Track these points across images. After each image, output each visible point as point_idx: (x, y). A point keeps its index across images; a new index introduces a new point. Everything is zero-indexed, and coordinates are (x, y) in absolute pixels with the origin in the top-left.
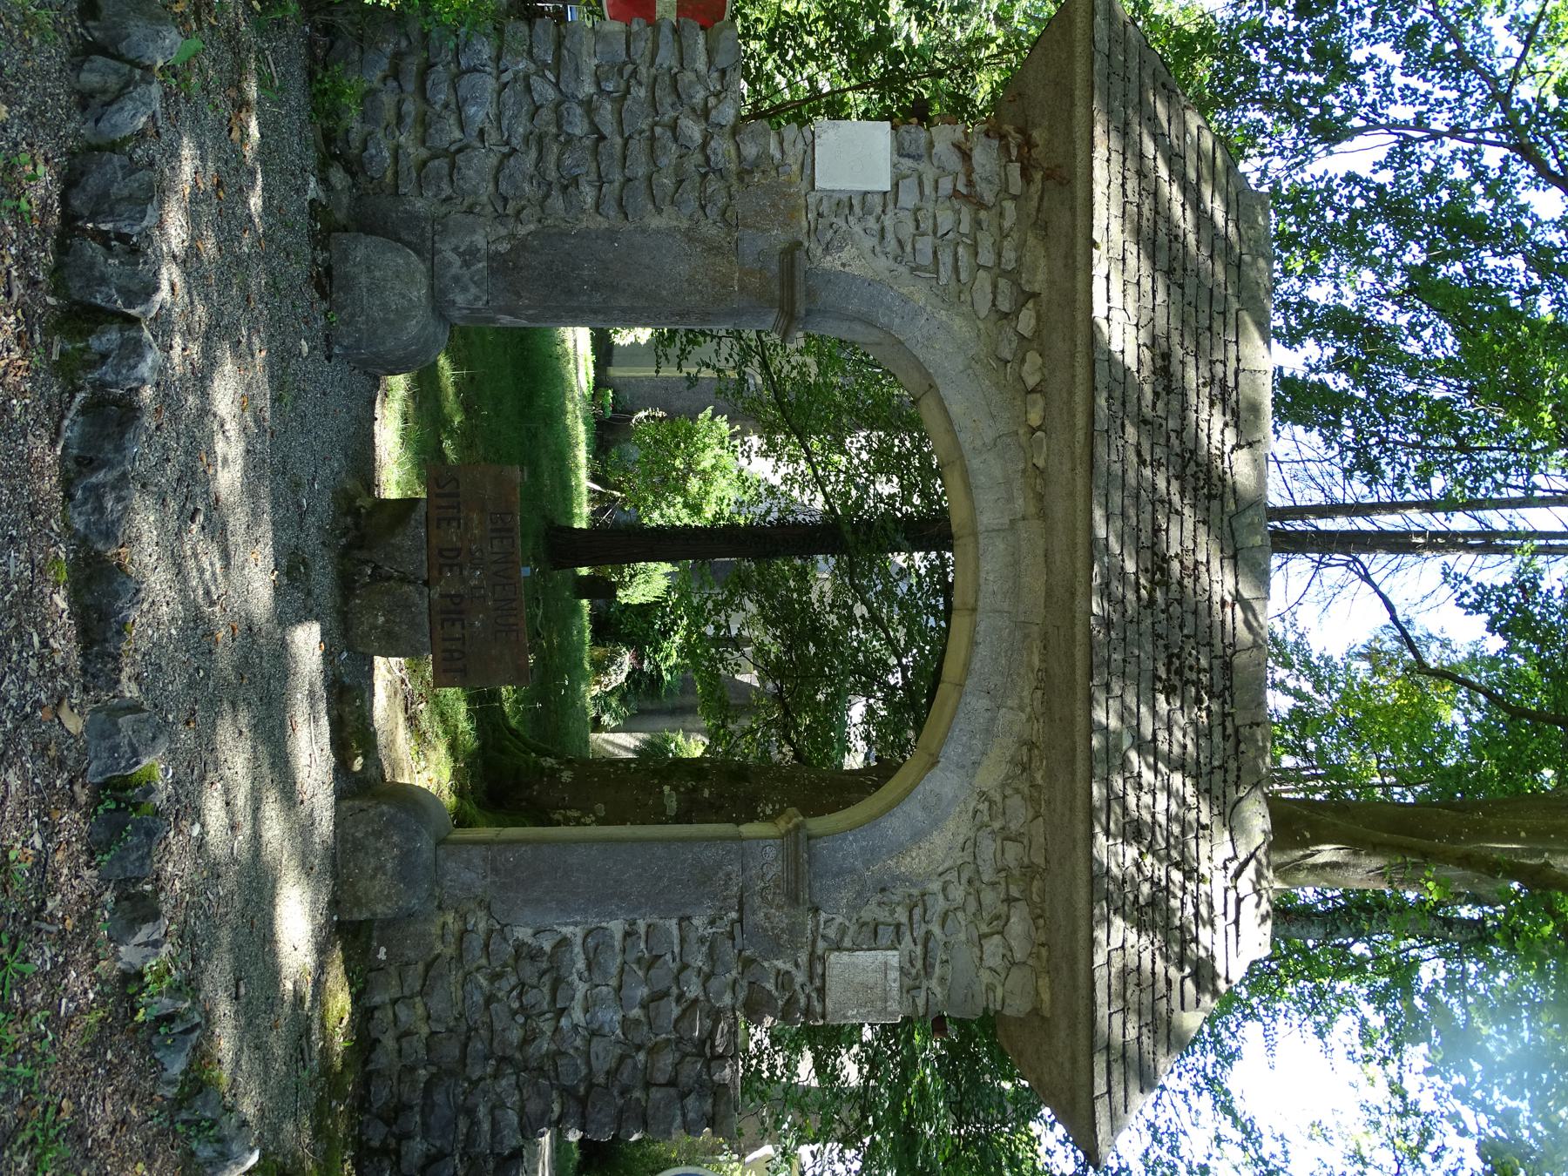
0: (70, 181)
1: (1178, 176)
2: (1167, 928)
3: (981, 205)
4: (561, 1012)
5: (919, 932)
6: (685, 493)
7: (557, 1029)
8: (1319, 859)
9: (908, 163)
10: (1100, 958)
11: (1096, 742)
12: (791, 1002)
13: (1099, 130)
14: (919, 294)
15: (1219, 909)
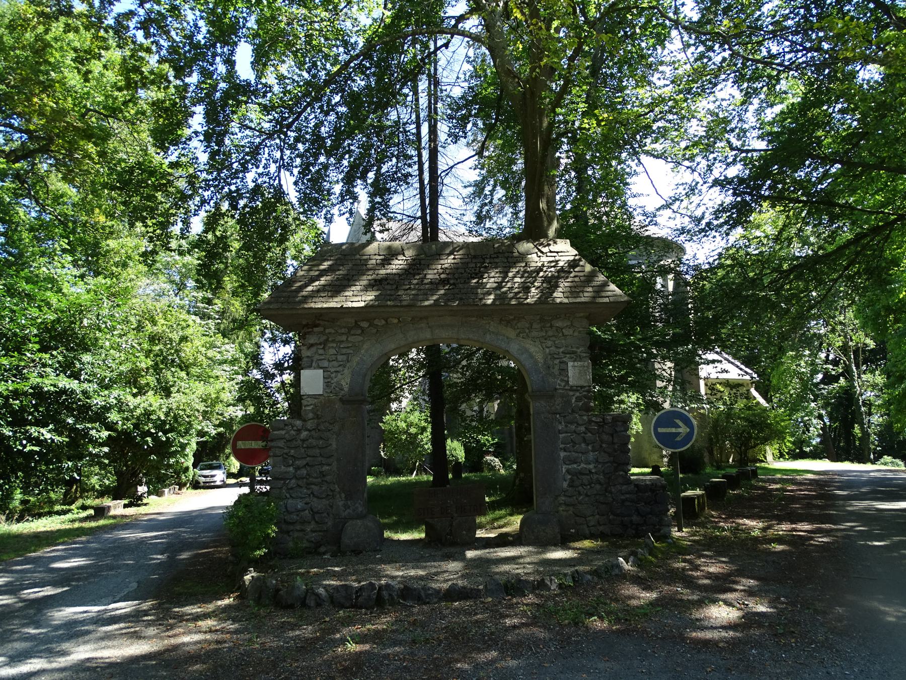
0: (342, 607)
1: (317, 278)
2: (559, 277)
3: (327, 340)
4: (590, 472)
5: (562, 355)
6: (416, 434)
7: (596, 473)
8: (545, 207)
9: (314, 364)
10: (566, 301)
11: (497, 303)
12: (585, 397)
13: (306, 306)
14: (356, 359)
15: (553, 259)
